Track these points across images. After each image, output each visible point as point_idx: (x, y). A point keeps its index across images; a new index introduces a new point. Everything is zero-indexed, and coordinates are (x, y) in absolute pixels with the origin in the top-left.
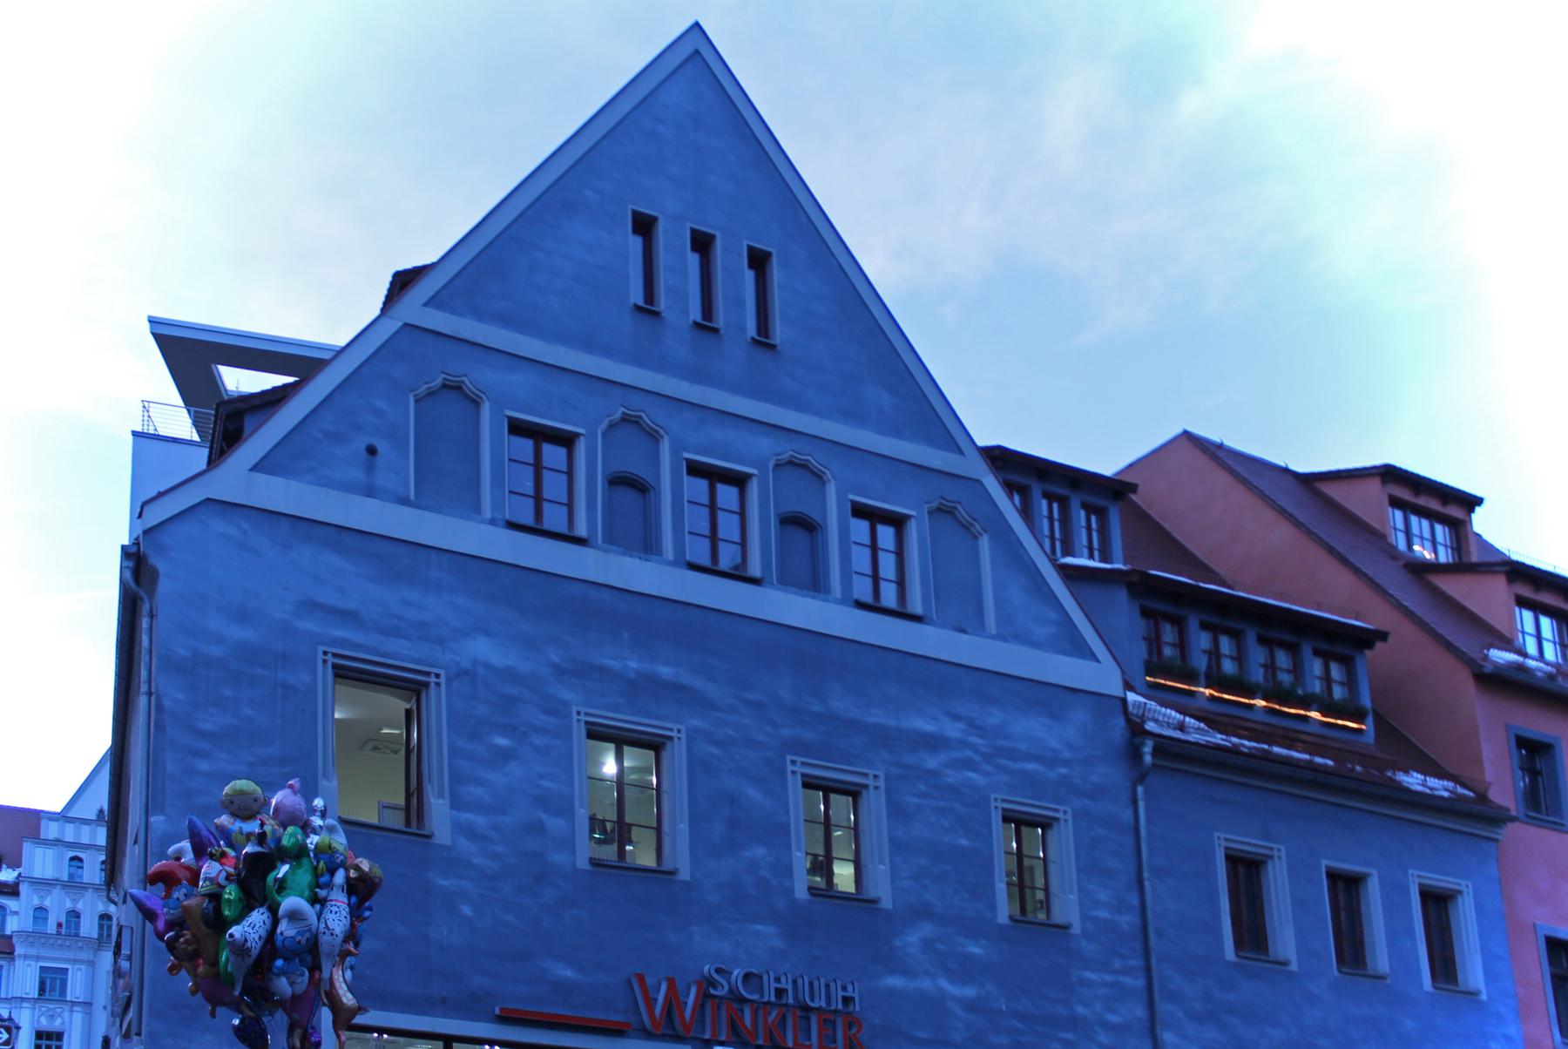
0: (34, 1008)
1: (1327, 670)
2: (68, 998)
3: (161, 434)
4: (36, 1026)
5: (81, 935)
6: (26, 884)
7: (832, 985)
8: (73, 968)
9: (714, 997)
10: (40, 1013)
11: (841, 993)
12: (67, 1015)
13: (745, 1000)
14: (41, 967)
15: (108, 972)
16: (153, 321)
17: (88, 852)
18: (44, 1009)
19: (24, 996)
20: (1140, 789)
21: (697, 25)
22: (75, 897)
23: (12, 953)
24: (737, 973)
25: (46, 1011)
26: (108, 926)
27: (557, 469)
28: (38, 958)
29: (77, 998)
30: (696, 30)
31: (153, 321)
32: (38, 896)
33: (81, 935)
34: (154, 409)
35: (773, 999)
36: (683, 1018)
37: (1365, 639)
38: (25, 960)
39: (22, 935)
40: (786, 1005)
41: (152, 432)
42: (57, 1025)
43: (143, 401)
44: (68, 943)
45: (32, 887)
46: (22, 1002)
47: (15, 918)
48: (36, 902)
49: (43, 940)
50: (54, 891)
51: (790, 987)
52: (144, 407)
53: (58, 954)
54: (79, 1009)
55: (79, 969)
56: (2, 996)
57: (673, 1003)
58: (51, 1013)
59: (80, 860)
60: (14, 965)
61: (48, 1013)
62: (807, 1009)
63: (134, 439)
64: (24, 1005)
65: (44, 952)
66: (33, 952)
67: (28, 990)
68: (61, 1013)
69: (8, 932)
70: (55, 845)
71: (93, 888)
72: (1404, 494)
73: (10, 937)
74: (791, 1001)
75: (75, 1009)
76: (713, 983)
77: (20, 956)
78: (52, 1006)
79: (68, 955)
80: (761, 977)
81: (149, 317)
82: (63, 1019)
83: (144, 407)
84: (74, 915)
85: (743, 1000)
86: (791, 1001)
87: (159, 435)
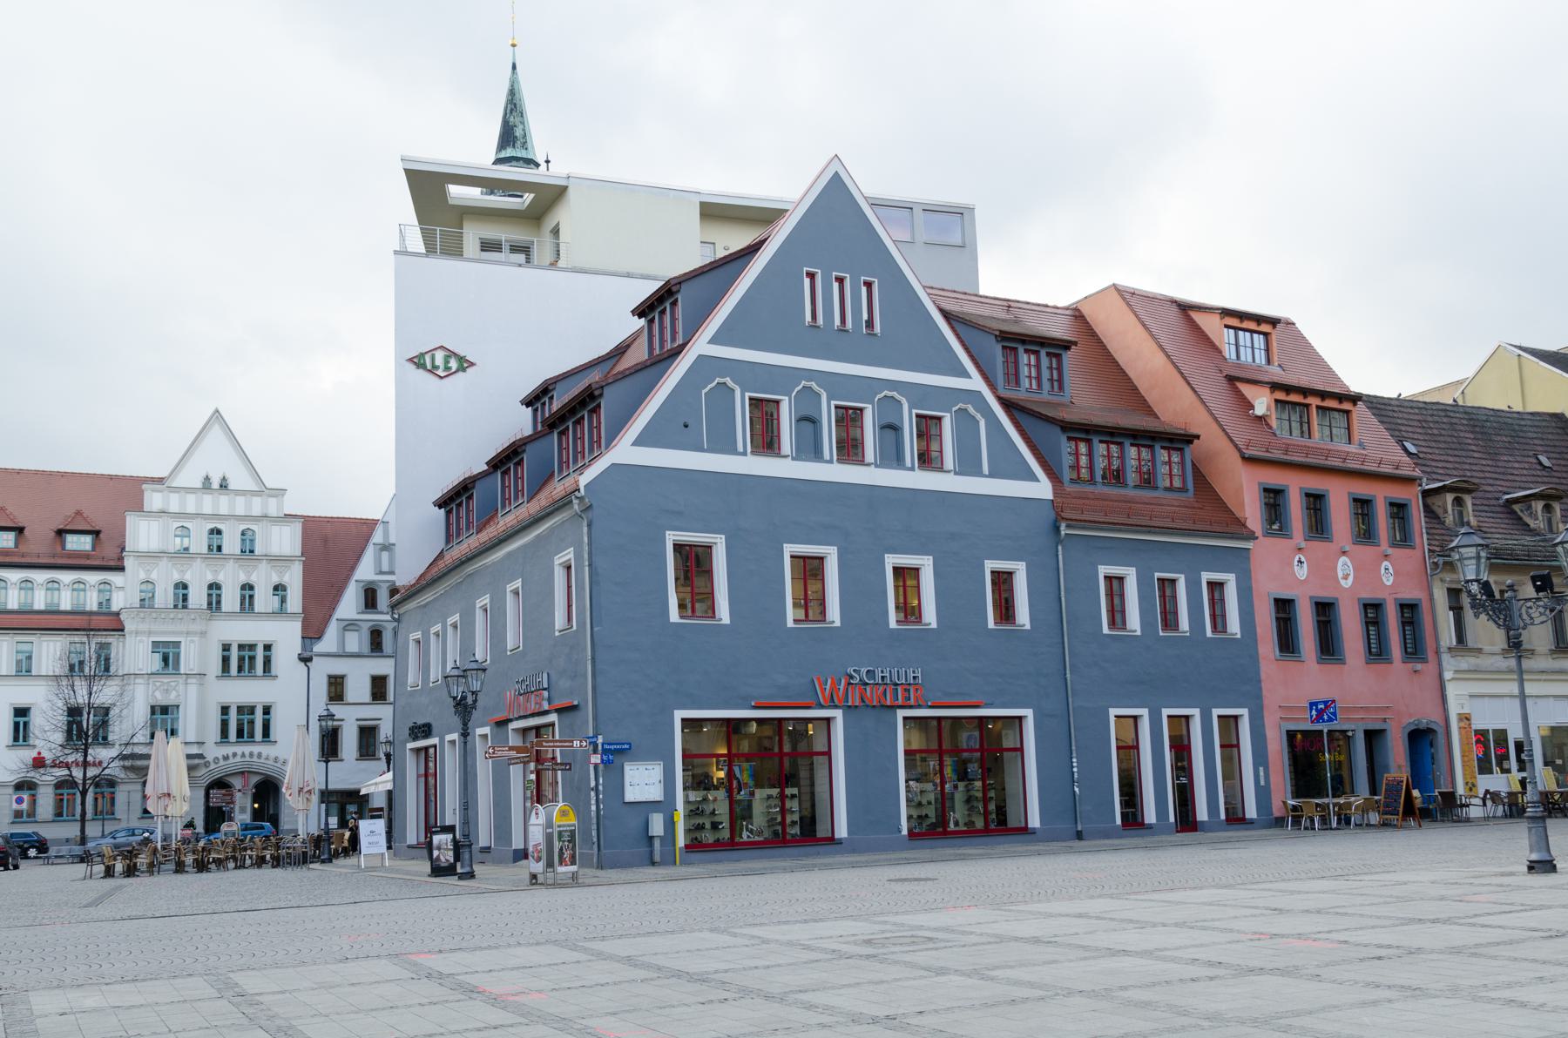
0: (149, 684)
1: (1170, 457)
2: (182, 672)
4: (151, 701)
5: (156, 606)
6: (131, 559)
7: (908, 671)
8: (186, 642)
9: (852, 684)
10: (154, 688)
11: (912, 675)
12: (181, 687)
13: (867, 684)
14: (153, 642)
18: (158, 684)
19: (188, 672)
20: (1060, 548)
22: (148, 567)
23: (123, 630)
24: (864, 670)
25: (160, 686)
26: (183, 595)
28: (150, 633)
29: (191, 670)
32: (143, 569)
33: (156, 606)
35: (880, 682)
36: (838, 696)
37: (1189, 439)
38: (136, 637)
39: (133, 612)
40: (886, 684)
42: (170, 699)
44: (180, 616)
46: (135, 678)
47: (121, 593)
48: (143, 576)
49: (154, 615)
50: (161, 563)
51: (888, 675)
53: (171, 628)
54: (194, 681)
55: (193, 641)
57: (834, 688)
58: (166, 688)
60: (124, 643)
61: (162, 688)
62: (896, 685)
64: (138, 681)
65: (154, 627)
66: (143, 627)
67: (140, 666)
68: (176, 686)
69: (115, 608)
70: (161, 517)
71: (134, 556)
72: (1235, 322)
73: (118, 614)
74: (888, 682)
75: (189, 681)
76: (851, 677)
77: (131, 632)
78: (166, 680)
79: (183, 627)
80: (874, 671)
81: (633, 312)
82: (177, 691)
85: (866, 684)
86: (888, 682)
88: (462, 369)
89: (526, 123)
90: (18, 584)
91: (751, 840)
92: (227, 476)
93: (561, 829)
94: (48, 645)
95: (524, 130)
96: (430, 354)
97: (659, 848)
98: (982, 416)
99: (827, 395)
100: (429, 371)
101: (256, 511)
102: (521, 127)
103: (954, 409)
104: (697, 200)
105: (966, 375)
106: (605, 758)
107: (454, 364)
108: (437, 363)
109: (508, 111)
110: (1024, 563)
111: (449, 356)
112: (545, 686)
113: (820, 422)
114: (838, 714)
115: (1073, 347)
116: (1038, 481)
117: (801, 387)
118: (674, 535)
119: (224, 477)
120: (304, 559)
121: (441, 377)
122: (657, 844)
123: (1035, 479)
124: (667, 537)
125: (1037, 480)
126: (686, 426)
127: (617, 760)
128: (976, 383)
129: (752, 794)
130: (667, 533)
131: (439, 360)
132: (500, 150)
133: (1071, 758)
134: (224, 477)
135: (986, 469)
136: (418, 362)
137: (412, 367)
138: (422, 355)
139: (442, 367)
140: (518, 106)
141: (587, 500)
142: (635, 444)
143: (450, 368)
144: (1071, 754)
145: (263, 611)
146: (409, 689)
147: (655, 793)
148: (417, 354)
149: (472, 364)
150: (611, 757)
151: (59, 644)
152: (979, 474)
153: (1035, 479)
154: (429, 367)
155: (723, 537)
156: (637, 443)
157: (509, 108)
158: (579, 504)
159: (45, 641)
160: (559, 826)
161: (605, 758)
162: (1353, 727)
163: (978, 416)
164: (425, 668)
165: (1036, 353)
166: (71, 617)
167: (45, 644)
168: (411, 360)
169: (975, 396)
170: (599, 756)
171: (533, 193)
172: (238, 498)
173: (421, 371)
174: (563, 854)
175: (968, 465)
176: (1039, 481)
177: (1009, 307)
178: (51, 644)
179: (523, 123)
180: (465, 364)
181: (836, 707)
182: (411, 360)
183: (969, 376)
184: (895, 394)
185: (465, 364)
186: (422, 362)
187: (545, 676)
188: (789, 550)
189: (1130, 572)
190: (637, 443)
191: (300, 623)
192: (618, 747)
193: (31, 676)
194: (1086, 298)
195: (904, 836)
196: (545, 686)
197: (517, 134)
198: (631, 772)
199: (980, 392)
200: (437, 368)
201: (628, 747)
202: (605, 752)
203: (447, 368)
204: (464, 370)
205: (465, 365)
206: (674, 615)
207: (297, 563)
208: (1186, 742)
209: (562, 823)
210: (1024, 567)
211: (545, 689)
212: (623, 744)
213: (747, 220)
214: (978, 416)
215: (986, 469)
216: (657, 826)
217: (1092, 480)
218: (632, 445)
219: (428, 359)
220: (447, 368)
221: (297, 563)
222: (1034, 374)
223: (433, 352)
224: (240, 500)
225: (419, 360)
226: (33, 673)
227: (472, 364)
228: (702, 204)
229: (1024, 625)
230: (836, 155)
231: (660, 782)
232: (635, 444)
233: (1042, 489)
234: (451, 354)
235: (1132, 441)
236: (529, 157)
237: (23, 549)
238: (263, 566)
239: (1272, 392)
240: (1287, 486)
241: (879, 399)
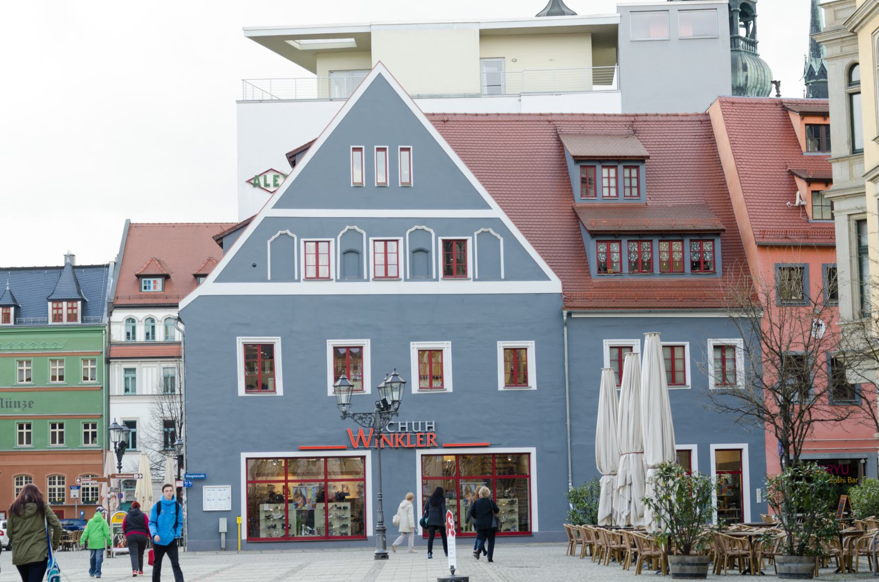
20: (565, 329)
90: (144, 321)
91: (308, 536)
93: (117, 526)
94: (152, 371)
96: (263, 176)
97: (224, 540)
105: (486, 206)
106: (186, 483)
108: (268, 182)
110: (534, 342)
111: (278, 176)
113: (362, 253)
114: (368, 454)
115: (646, 161)
116: (548, 279)
117: (346, 230)
118: (242, 339)
122: (223, 537)
124: (238, 340)
126: (254, 266)
127: (197, 484)
128: (496, 211)
129: (314, 506)
130: (238, 338)
131: (270, 180)
133: (569, 483)
135: (503, 277)
136: (254, 182)
137: (250, 186)
138: (257, 177)
139: (272, 184)
142: (215, 281)
144: (568, 479)
147: (226, 506)
148: (254, 176)
150: (190, 483)
151: (155, 369)
152: (498, 278)
154: (262, 185)
155: (280, 338)
159: (145, 367)
160: (114, 525)
161: (186, 483)
162: (865, 456)
163: (498, 236)
165: (616, 167)
166: (163, 347)
167: (145, 369)
168: (249, 181)
169: (496, 223)
170: (182, 482)
173: (257, 189)
174: (118, 541)
175: (488, 273)
176: (550, 280)
178: (150, 369)
181: (366, 449)
182: (249, 181)
186: (257, 182)
188: (331, 343)
189: (635, 343)
192: (197, 476)
193: (136, 395)
195: (420, 536)
198: (208, 492)
199: (499, 218)
201: (203, 476)
202: (187, 479)
206: (241, 391)
208: (849, 462)
209: (116, 523)
212: (200, 475)
213: (523, 35)
214: (498, 236)
216: (223, 527)
217: (621, 273)
219: (262, 180)
223: (266, 174)
225: (255, 181)
226: (137, 393)
230: (380, 61)
231: (229, 498)
232: (215, 281)
233: (553, 285)
235: (661, 239)
237: (168, 292)
239: (809, 185)
240: (808, 264)
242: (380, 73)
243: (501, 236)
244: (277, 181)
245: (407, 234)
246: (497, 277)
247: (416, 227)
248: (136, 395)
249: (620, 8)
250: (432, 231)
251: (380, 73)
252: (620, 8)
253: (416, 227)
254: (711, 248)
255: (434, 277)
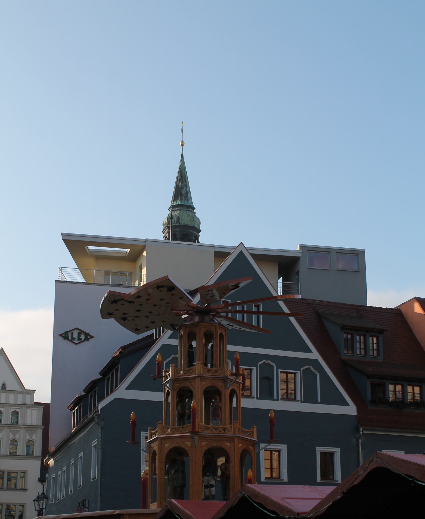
3: (68, 280)
15: (42, 487)
16: (63, 234)
17: (160, 510)
21: (241, 243)
27: (271, 286)
30: (241, 244)
31: (63, 234)
34: (63, 270)
41: (63, 280)
43: (59, 267)
45: (25, 430)
52: (59, 269)
56: (1, 454)
59: (18, 413)
63: (62, 236)
71: (7, 426)
83: (59, 269)
84: (14, 442)
87: (67, 281)
88: (87, 339)
89: (188, 187)
92: (6, 383)
95: (186, 190)
96: (71, 332)
98: (318, 372)
99: (231, 363)
100: (70, 341)
101: (20, 401)
102: (185, 188)
103: (302, 369)
104: (213, 251)
105: (310, 351)
107: (83, 337)
109: (178, 180)
110: (339, 448)
112: (87, 506)
119: (4, 383)
120: (43, 427)
121: (76, 344)
123: (347, 404)
124: (142, 434)
125: (348, 405)
128: (315, 355)
130: (142, 432)
131: (75, 335)
132: (174, 202)
134: (4, 383)
135: (319, 400)
137: (61, 338)
138: (67, 333)
139: (77, 338)
140: (184, 177)
141: (101, 416)
143: (81, 339)
145: (21, 455)
146: (50, 503)
149: (92, 337)
152: (316, 402)
153: (347, 404)
154: (70, 338)
156: (128, 388)
157: (179, 178)
158: (97, 418)
163: (316, 372)
164: (218, 479)
169: (315, 362)
171: (129, 249)
172: (11, 394)
173: (66, 341)
177: (358, 309)
179: (186, 186)
180: (88, 337)
182: (61, 335)
183: (311, 352)
184: (269, 361)
185: (88, 337)
186: (66, 336)
187: (87, 501)
190: (128, 388)
191: (40, 461)
193: (16, 489)
194: (403, 304)
196: (87, 506)
197: (183, 192)
200: (74, 339)
203: (79, 339)
204: (88, 340)
205: (89, 337)
207: (40, 429)
210: (339, 451)
211: (87, 508)
214: (316, 372)
215: (319, 400)
218: (125, 389)
220: (79, 339)
221: (40, 429)
222: (362, 346)
223: (73, 331)
224: (12, 396)
225: (65, 335)
227: (92, 337)
228: (216, 252)
229: (338, 481)
234: (81, 332)
236: (189, 204)
238: (22, 431)
241: (260, 364)
242: (241, 251)
243: (318, 372)
244: (80, 336)
245: (258, 365)
246: (315, 401)
247: (264, 361)
248: (16, 489)
249: (301, 247)
250: (274, 365)
251: (241, 251)
252: (301, 247)
253: (264, 361)
254: (277, 452)
255: (275, 397)
